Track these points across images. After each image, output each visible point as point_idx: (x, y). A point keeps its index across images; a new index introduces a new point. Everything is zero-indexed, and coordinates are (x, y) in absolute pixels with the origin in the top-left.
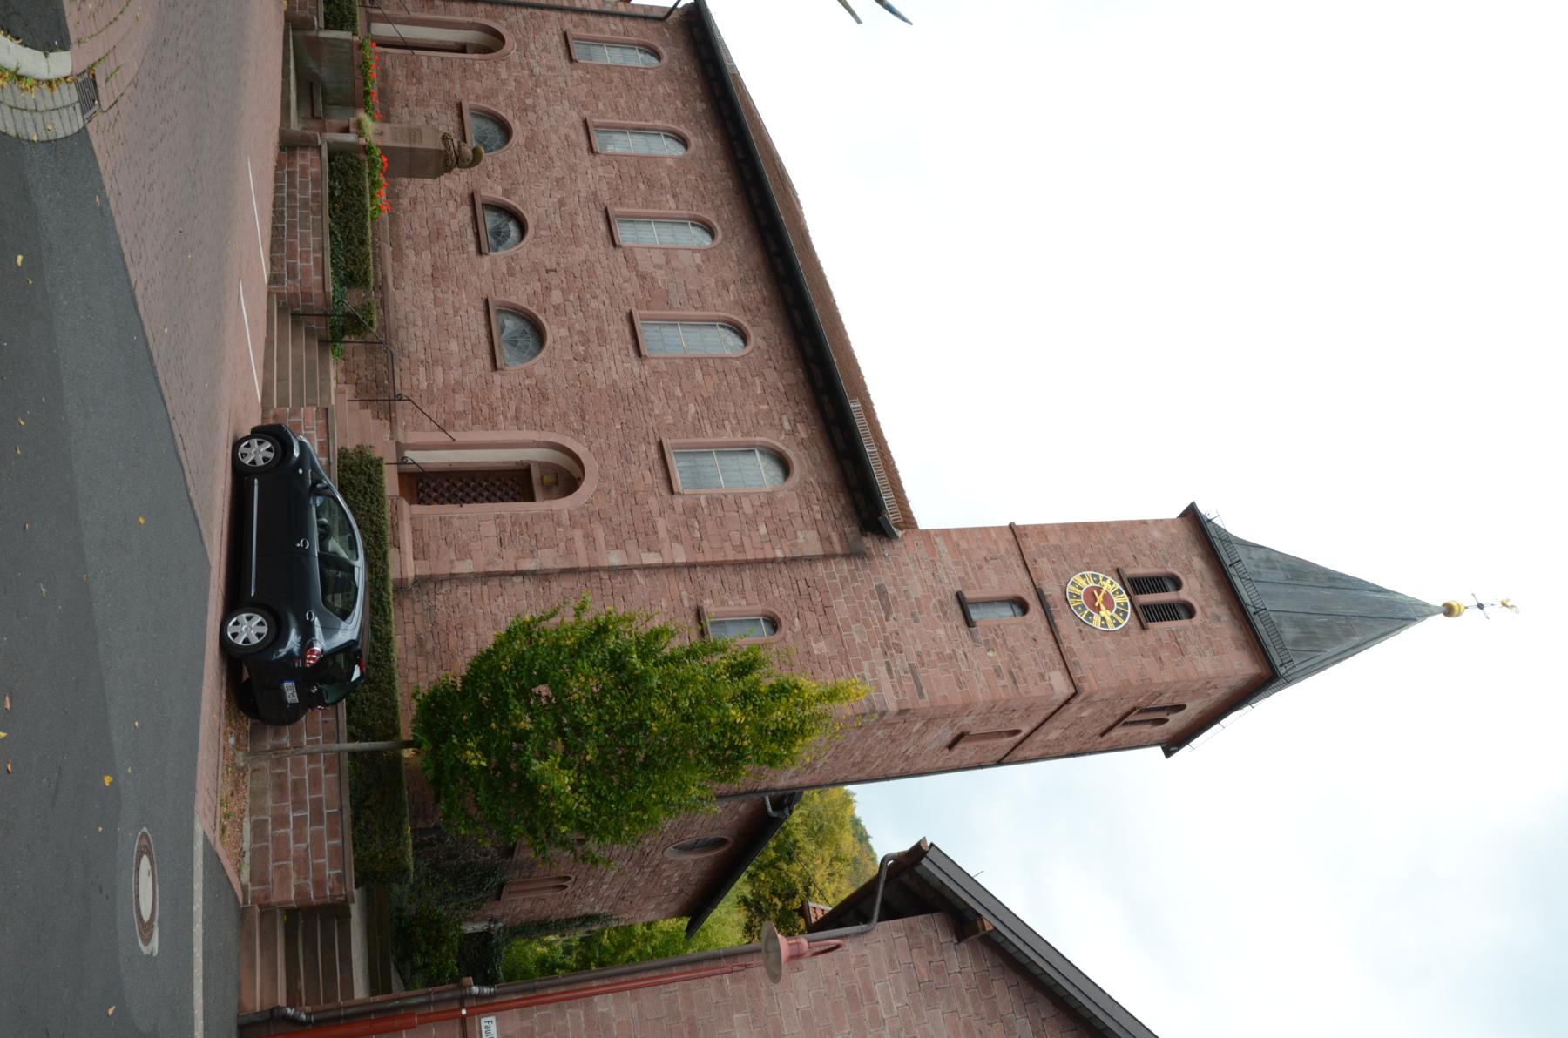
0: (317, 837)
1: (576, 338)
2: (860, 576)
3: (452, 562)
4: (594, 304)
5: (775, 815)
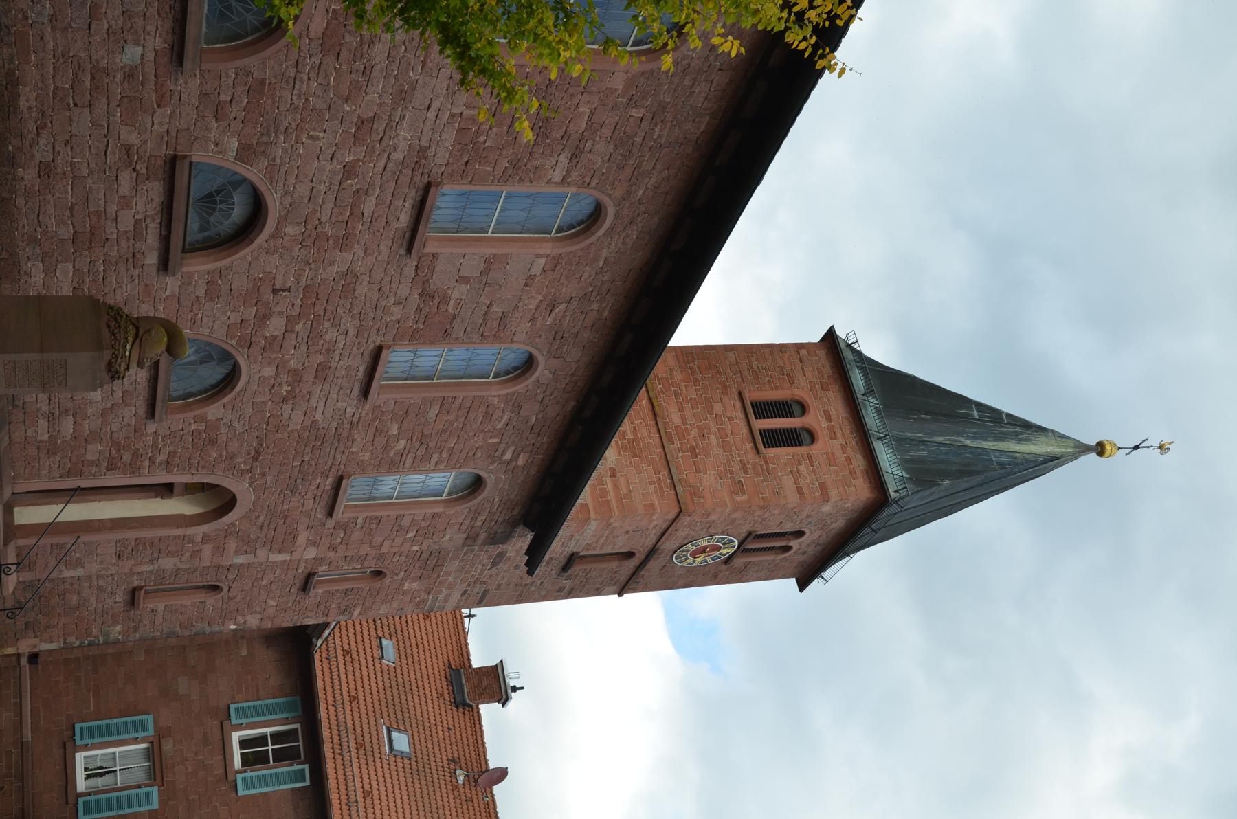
1: (284, 377)
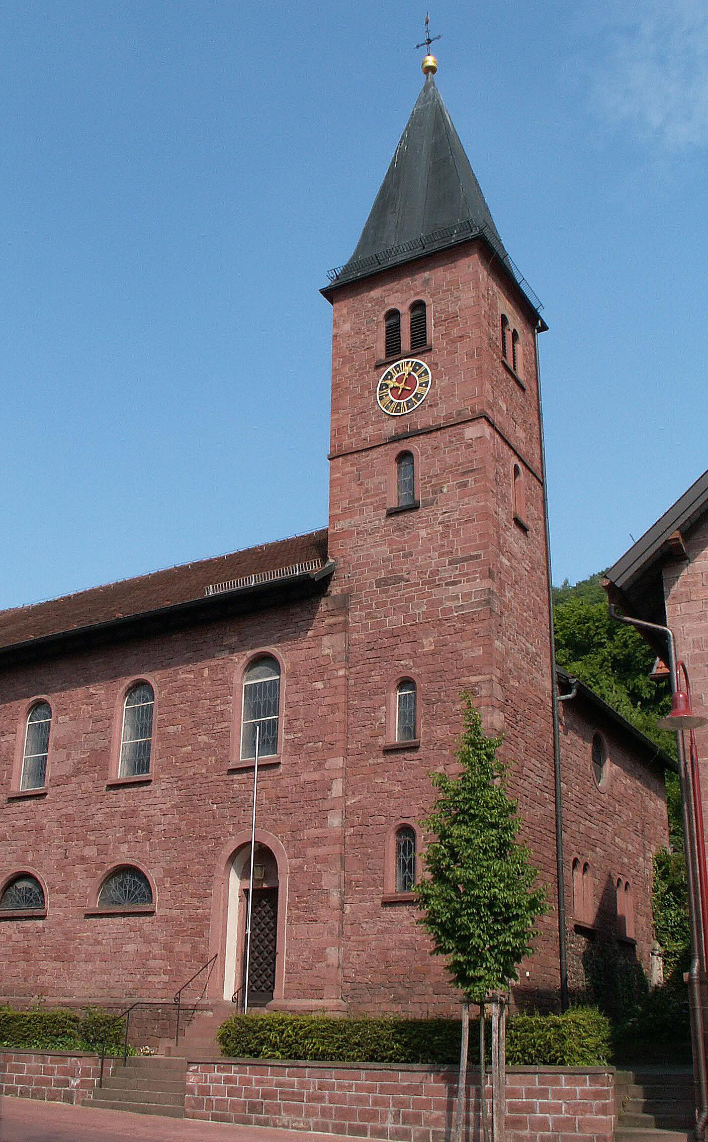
0: (558, 1095)
2: (367, 601)
3: (328, 966)
4: (99, 818)
5: (574, 691)
